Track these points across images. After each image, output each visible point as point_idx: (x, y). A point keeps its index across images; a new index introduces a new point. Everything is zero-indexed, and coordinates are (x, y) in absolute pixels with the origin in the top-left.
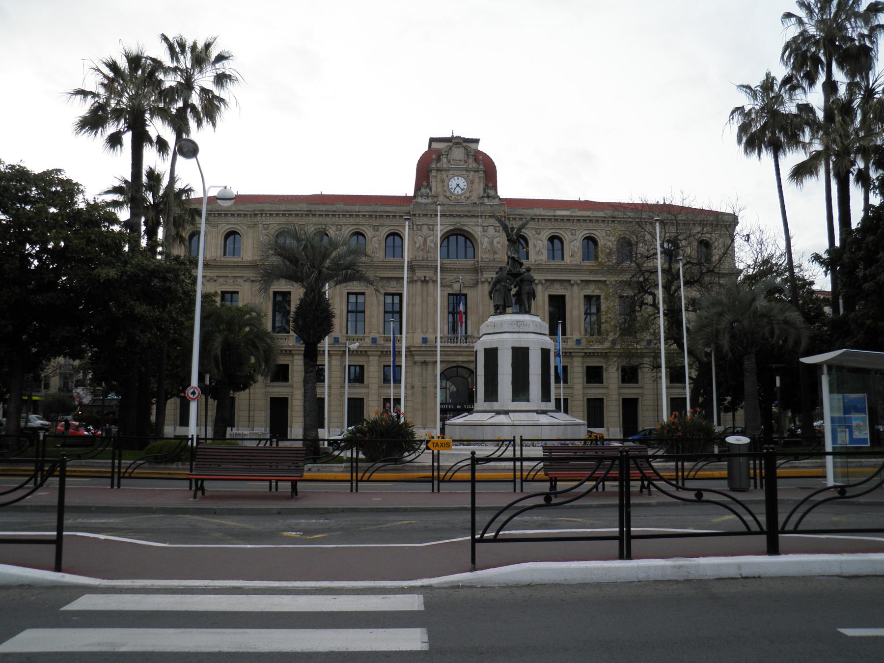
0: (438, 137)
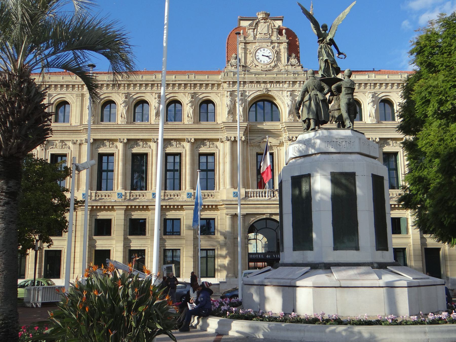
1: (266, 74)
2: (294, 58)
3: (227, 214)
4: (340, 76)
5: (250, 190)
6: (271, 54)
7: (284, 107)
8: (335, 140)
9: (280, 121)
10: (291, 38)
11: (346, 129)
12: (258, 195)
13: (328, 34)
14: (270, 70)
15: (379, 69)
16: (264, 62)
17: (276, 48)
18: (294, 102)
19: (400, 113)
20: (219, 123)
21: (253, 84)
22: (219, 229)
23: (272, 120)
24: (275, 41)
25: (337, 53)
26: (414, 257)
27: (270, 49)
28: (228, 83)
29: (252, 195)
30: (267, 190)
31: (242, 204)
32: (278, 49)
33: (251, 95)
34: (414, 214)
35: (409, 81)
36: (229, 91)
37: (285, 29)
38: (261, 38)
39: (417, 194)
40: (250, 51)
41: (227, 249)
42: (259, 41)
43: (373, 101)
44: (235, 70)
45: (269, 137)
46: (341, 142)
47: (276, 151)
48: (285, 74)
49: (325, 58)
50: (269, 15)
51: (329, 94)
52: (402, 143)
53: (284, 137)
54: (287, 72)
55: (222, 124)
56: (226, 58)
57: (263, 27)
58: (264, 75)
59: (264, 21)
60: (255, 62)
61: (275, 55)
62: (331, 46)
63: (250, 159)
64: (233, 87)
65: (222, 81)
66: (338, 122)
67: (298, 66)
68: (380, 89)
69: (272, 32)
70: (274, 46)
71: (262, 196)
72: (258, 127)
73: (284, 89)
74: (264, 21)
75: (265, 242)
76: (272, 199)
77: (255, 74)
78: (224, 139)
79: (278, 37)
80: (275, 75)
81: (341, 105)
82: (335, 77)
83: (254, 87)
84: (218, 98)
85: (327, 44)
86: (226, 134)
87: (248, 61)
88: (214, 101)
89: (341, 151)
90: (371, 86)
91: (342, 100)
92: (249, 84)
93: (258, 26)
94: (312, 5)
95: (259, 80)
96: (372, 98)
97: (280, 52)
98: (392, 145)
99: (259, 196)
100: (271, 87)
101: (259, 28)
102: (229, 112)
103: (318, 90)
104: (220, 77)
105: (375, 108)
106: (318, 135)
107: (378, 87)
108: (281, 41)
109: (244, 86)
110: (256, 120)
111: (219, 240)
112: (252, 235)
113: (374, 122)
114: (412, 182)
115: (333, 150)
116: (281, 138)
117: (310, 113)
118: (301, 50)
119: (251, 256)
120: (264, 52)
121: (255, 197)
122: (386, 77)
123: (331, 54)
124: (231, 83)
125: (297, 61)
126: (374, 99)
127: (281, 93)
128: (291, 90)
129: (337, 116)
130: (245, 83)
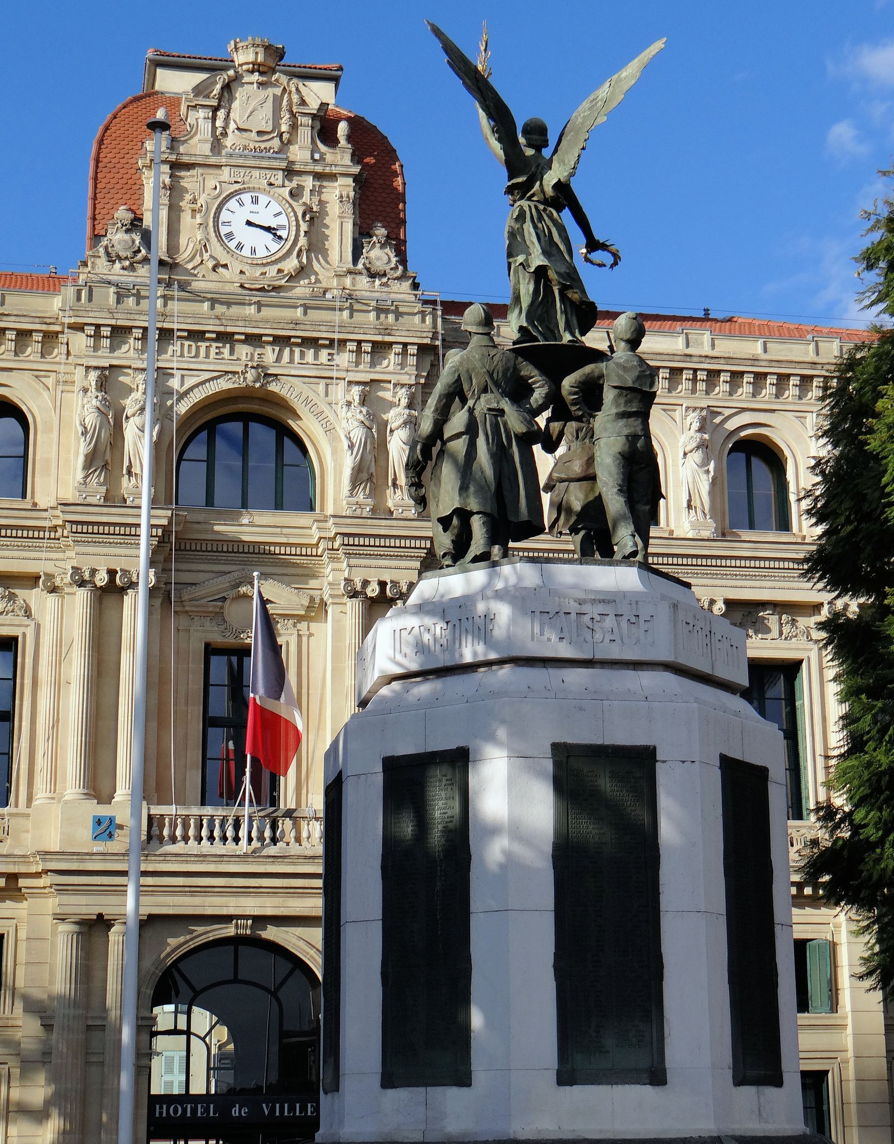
0: (584, 210)
1: (259, 305)
2: (383, 246)
3: (61, 918)
4: (595, 339)
5: (170, 810)
6: (282, 220)
7: (334, 452)
8: (573, 607)
9: (312, 509)
10: (370, 160)
11: (618, 563)
12: (204, 833)
13: (551, 160)
14: (276, 289)
15: (731, 315)
16: (253, 251)
17: (306, 198)
18: (378, 431)
19: (816, 500)
20: (42, 505)
21: (203, 345)
22: (20, 983)
23: (279, 505)
24: (302, 168)
25: (584, 241)
26: (861, 1115)
27: (280, 199)
28: (90, 330)
29: (178, 832)
30: (246, 810)
31: (145, 874)
32: (316, 199)
33: (191, 389)
34: (867, 927)
35: (853, 371)
36: (96, 368)
37: (349, 120)
38: (245, 148)
39: (881, 842)
40: (194, 201)
41: (53, 1079)
42: (233, 161)
43: (702, 445)
44: (127, 278)
45: (264, 576)
46: (598, 618)
47: (293, 641)
48: (341, 310)
49: (538, 260)
50: (280, 54)
51: (547, 414)
52: (822, 626)
53: (330, 578)
54: (351, 301)
55: (58, 512)
56: (89, 223)
57: (253, 103)
58: (253, 309)
59: (261, 79)
60: (216, 248)
61: (304, 227)
62: (559, 211)
63: (176, 669)
64: (113, 349)
65: (67, 321)
66: (582, 533)
67: (397, 279)
68: (731, 394)
69: (294, 127)
70: (300, 188)
71: (224, 839)
72: (218, 533)
73: (335, 374)
74: (261, 79)
75: (220, 1048)
76: (265, 852)
77: (213, 302)
78: (64, 579)
79: (319, 151)
80: (299, 311)
81: (598, 459)
82: (578, 341)
83: (207, 356)
84: (45, 394)
85: (546, 202)
86: (71, 554)
87: (183, 241)
88: (24, 408)
89: (599, 656)
90: (695, 380)
91: (602, 442)
92: (187, 343)
93: (231, 99)
94: (485, 37)
95: (230, 329)
96: (701, 430)
97: (323, 212)
98: (775, 633)
99: (211, 838)
100: (278, 359)
101: (236, 105)
102: (90, 461)
103: (504, 394)
104: (57, 303)
105: (712, 473)
106: (500, 585)
107: (723, 387)
108: (327, 170)
109: (161, 351)
110: (210, 501)
111: (19, 1035)
112: (165, 1015)
113: (706, 534)
114: (864, 791)
115: (565, 651)
116: (313, 583)
117: (472, 489)
118: (412, 211)
119: (162, 1111)
120: (254, 207)
121: (191, 842)
122: (756, 348)
123: (562, 247)
124: (106, 331)
125: (394, 260)
126: (706, 436)
127: (321, 387)
128: (366, 377)
129: (577, 506)
130: (166, 335)
